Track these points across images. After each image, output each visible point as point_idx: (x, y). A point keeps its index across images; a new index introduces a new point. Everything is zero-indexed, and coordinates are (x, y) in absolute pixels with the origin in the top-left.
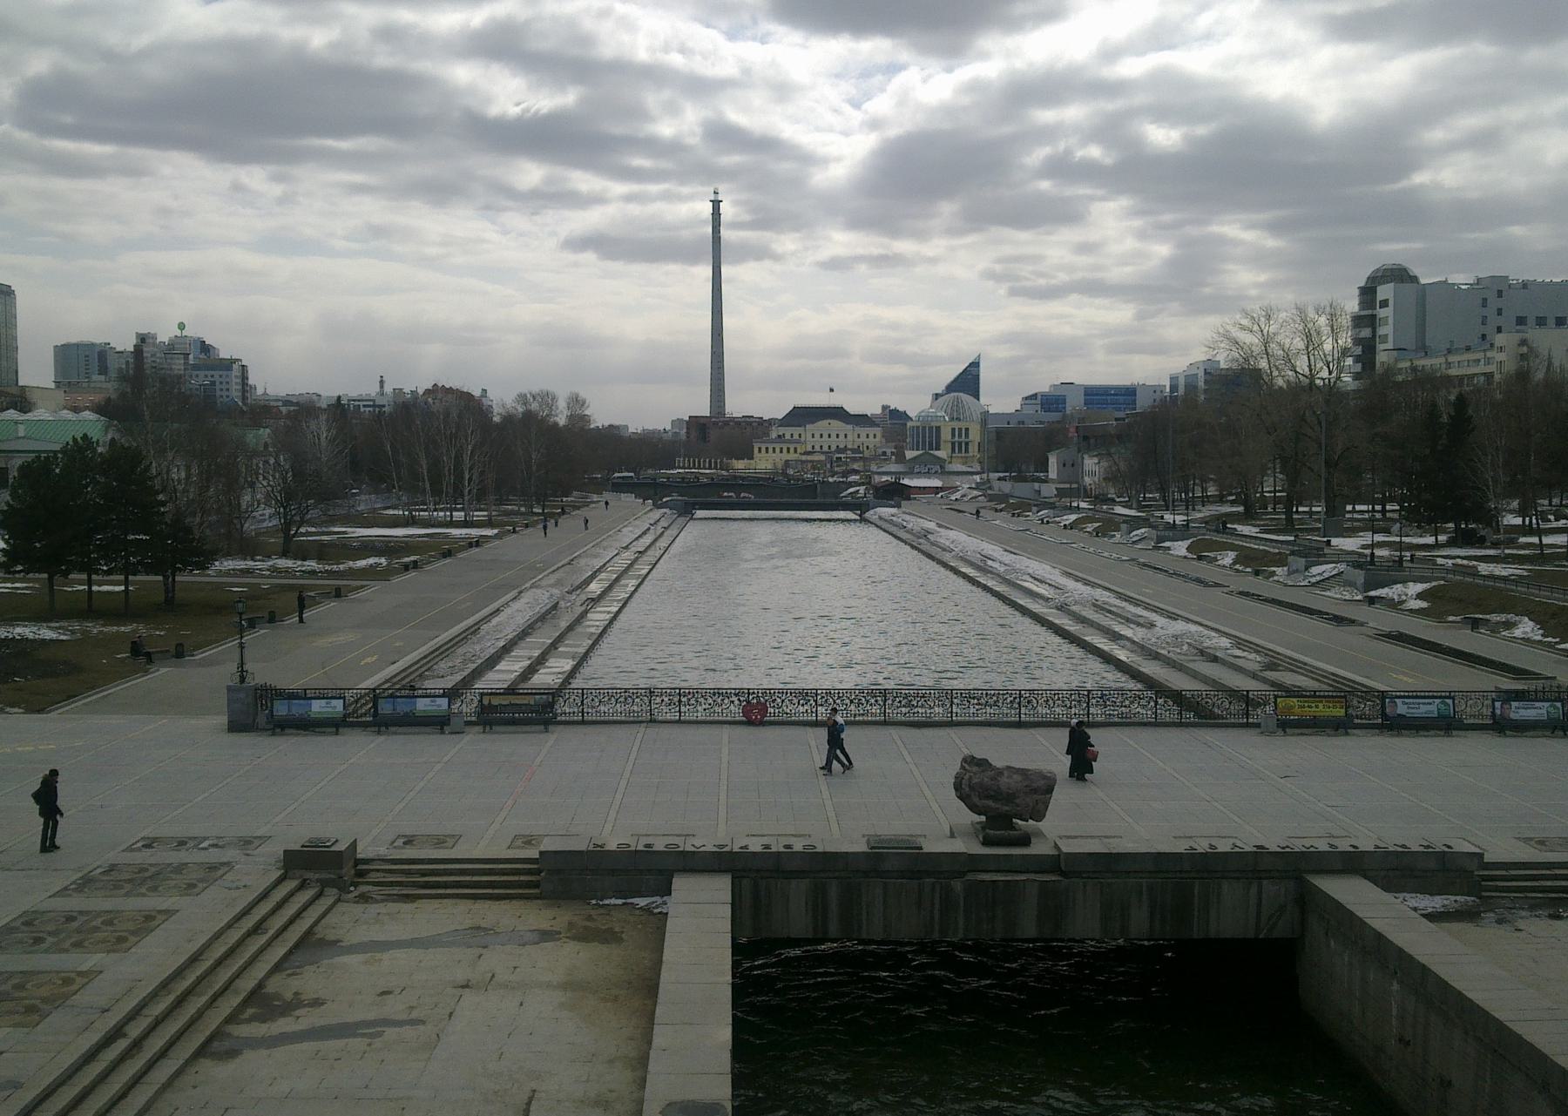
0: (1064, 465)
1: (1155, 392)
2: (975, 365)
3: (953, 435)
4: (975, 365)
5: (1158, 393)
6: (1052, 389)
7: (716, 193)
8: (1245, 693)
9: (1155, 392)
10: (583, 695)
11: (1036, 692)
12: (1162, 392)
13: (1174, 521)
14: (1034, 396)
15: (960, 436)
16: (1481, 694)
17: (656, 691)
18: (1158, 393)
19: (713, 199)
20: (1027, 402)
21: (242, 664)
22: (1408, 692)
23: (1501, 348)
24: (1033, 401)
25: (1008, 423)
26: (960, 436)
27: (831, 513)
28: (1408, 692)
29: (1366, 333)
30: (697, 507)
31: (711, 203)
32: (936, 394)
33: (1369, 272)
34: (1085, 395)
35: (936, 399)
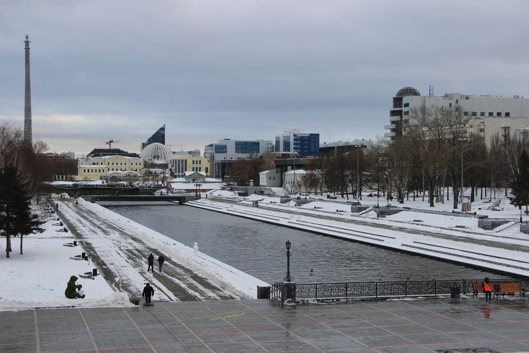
1: (268, 144)
2: (163, 129)
3: (193, 163)
4: (163, 129)
5: (269, 144)
6: (220, 142)
7: (27, 37)
9: (268, 144)
10: (406, 285)
11: (449, 282)
12: (271, 144)
13: (378, 205)
14: (211, 145)
15: (197, 163)
16: (338, 285)
17: (466, 281)
18: (269, 144)
19: (25, 40)
20: (209, 148)
21: (288, 273)
22: (332, 284)
23: (471, 126)
24: (211, 148)
25: (232, 158)
26: (197, 163)
27: (132, 202)
28: (332, 284)
29: (397, 118)
30: (98, 199)
31: (24, 43)
32: (143, 144)
33: (402, 87)
34: (236, 145)
35: (143, 148)
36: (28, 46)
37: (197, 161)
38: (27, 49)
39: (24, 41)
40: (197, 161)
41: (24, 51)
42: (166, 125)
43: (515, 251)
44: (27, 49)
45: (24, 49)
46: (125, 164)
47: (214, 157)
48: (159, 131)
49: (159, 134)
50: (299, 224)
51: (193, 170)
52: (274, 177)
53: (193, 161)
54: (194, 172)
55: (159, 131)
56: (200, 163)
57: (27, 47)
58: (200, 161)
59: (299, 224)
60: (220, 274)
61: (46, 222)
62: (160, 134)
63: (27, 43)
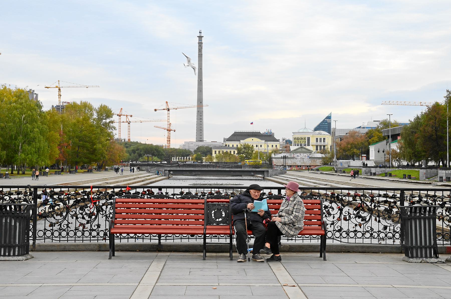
0: (379, 151)
4: (329, 117)
8: (168, 142)
15: (321, 141)
19: (199, 36)
26: (321, 141)
36: (201, 40)
37: (321, 139)
38: (200, 44)
39: (198, 37)
40: (321, 139)
41: (197, 45)
42: (332, 115)
43: (442, 101)
44: (200, 44)
45: (198, 44)
46: (261, 146)
47: (334, 132)
48: (325, 120)
49: (326, 123)
50: (229, 179)
51: (298, 145)
52: (383, 150)
53: (317, 139)
54: (298, 147)
55: (325, 120)
56: (324, 141)
57: (200, 42)
58: (324, 139)
59: (229, 179)
60: (71, 224)
61: (283, 216)
62: (326, 122)
63: (200, 37)
